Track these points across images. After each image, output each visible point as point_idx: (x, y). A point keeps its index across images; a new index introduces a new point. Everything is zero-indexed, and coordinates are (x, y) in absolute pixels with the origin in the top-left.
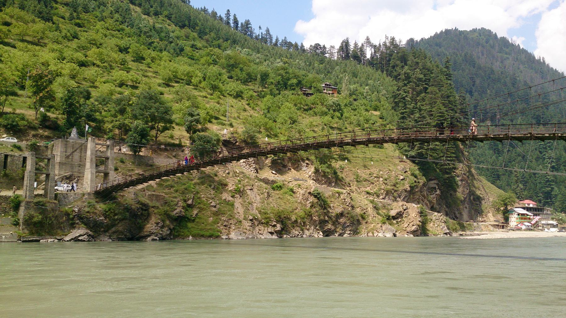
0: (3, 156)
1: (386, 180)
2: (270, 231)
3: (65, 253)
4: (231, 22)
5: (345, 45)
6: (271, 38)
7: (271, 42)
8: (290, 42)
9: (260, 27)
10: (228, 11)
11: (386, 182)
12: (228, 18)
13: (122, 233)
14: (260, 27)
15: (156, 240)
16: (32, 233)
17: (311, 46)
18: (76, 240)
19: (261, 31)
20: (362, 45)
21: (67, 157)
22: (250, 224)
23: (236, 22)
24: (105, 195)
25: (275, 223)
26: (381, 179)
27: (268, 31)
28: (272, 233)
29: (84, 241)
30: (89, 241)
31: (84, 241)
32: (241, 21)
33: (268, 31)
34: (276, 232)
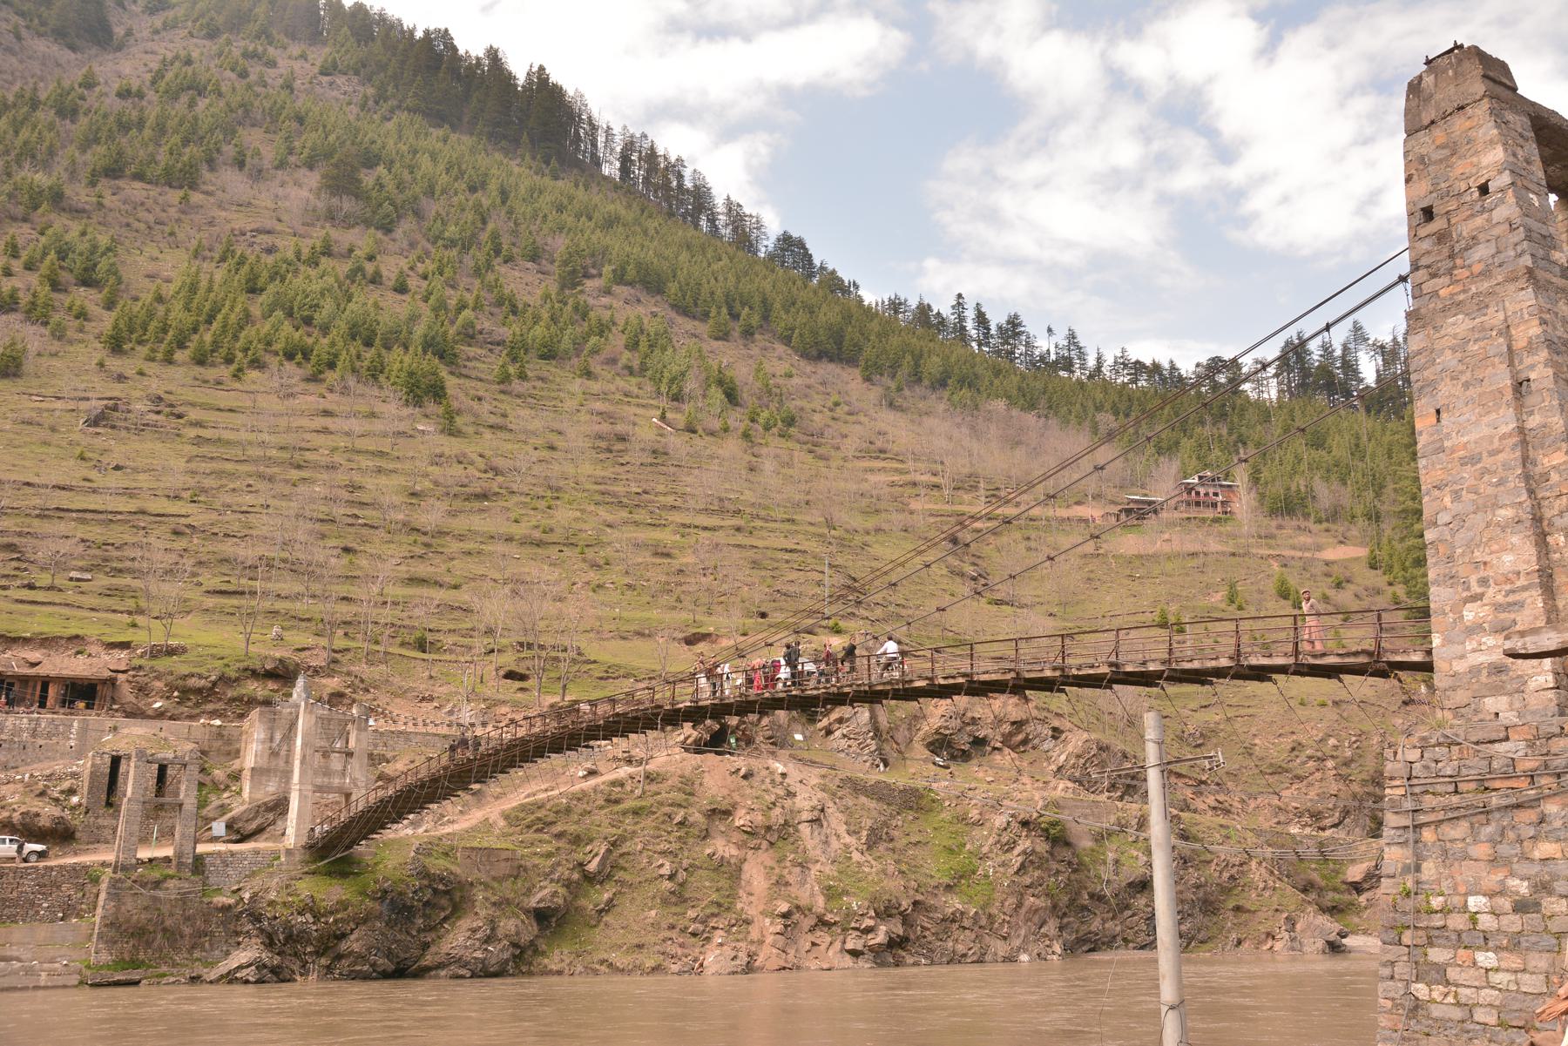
0: (108, 760)
1: (1347, 764)
2: (849, 946)
3: (396, 1037)
4: (970, 325)
5: (1294, 353)
6: (1082, 355)
7: (1083, 367)
8: (1137, 362)
9: (1050, 330)
10: (960, 296)
11: (1344, 770)
12: (961, 319)
13: (361, 957)
14: (1050, 330)
15: (462, 977)
16: (121, 964)
17: (1198, 365)
18: (230, 978)
19: (1054, 339)
20: (1345, 348)
21: (274, 754)
22: (779, 928)
23: (981, 319)
24: (334, 850)
25: (871, 923)
26: (1330, 764)
27: (1072, 336)
28: (855, 954)
29: (247, 982)
30: (260, 981)
31: (247, 982)
32: (996, 319)
33: (1072, 336)
34: (871, 949)
